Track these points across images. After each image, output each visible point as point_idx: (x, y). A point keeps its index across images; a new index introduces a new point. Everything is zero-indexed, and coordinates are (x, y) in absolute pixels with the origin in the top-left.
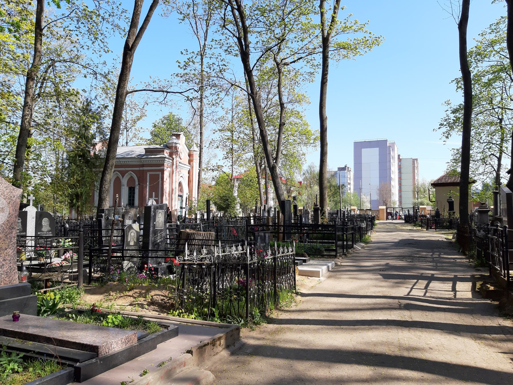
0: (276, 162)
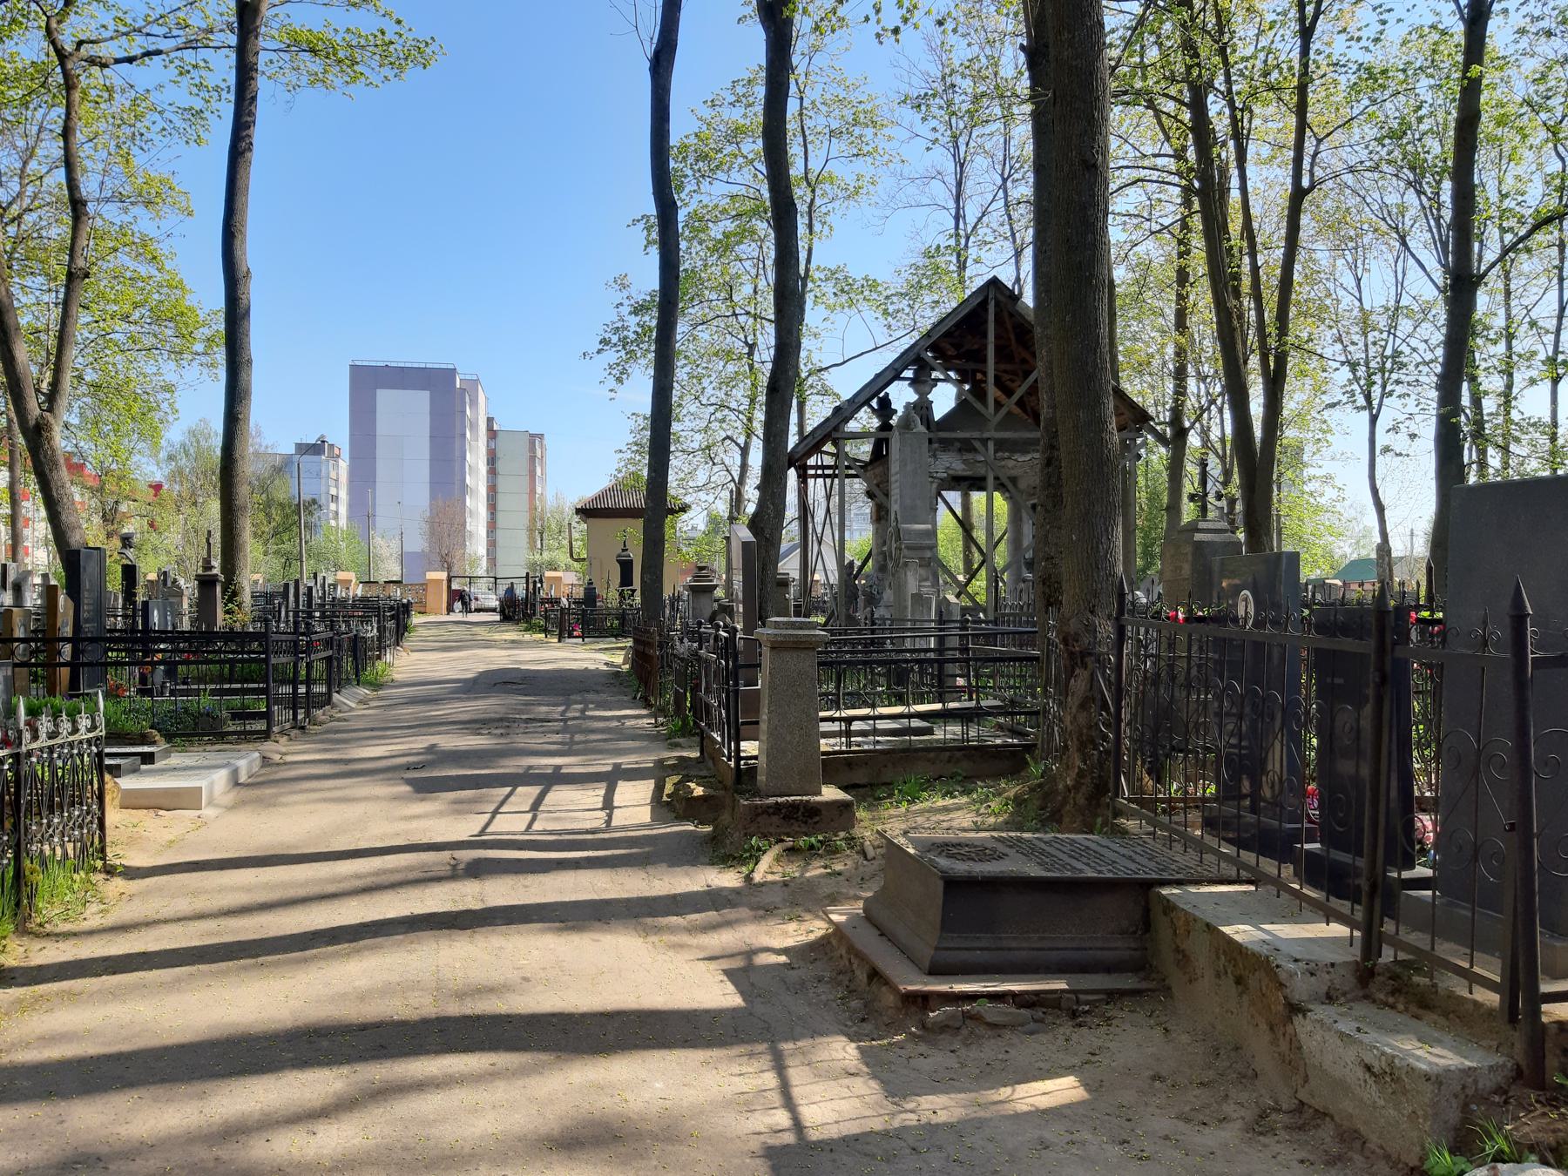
0: (50, 410)
